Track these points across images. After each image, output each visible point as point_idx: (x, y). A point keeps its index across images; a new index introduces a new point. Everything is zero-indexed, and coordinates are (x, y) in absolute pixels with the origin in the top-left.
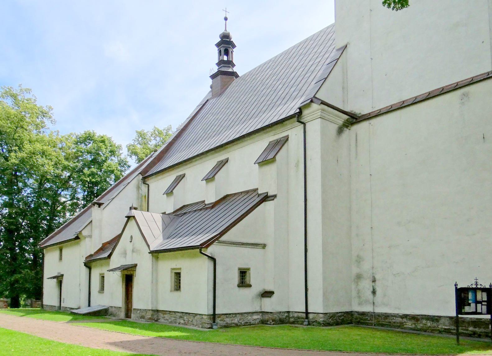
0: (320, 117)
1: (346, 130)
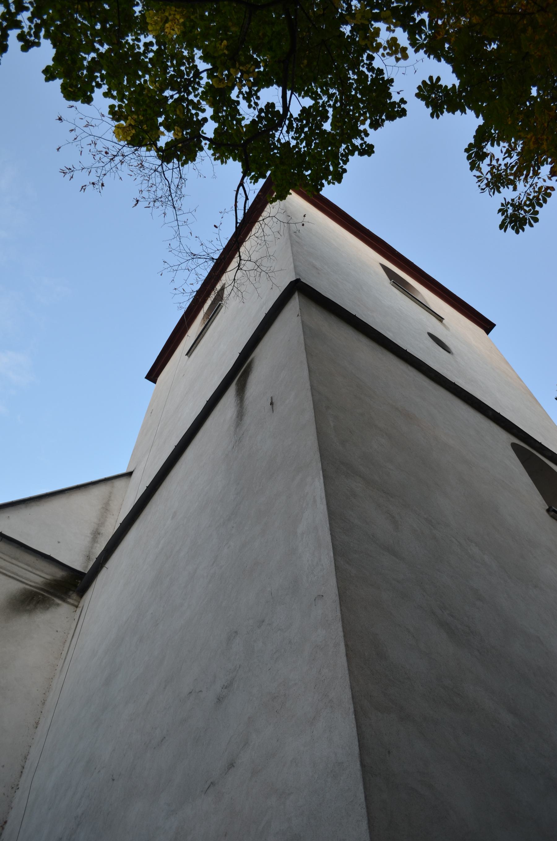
1: (58, 605)
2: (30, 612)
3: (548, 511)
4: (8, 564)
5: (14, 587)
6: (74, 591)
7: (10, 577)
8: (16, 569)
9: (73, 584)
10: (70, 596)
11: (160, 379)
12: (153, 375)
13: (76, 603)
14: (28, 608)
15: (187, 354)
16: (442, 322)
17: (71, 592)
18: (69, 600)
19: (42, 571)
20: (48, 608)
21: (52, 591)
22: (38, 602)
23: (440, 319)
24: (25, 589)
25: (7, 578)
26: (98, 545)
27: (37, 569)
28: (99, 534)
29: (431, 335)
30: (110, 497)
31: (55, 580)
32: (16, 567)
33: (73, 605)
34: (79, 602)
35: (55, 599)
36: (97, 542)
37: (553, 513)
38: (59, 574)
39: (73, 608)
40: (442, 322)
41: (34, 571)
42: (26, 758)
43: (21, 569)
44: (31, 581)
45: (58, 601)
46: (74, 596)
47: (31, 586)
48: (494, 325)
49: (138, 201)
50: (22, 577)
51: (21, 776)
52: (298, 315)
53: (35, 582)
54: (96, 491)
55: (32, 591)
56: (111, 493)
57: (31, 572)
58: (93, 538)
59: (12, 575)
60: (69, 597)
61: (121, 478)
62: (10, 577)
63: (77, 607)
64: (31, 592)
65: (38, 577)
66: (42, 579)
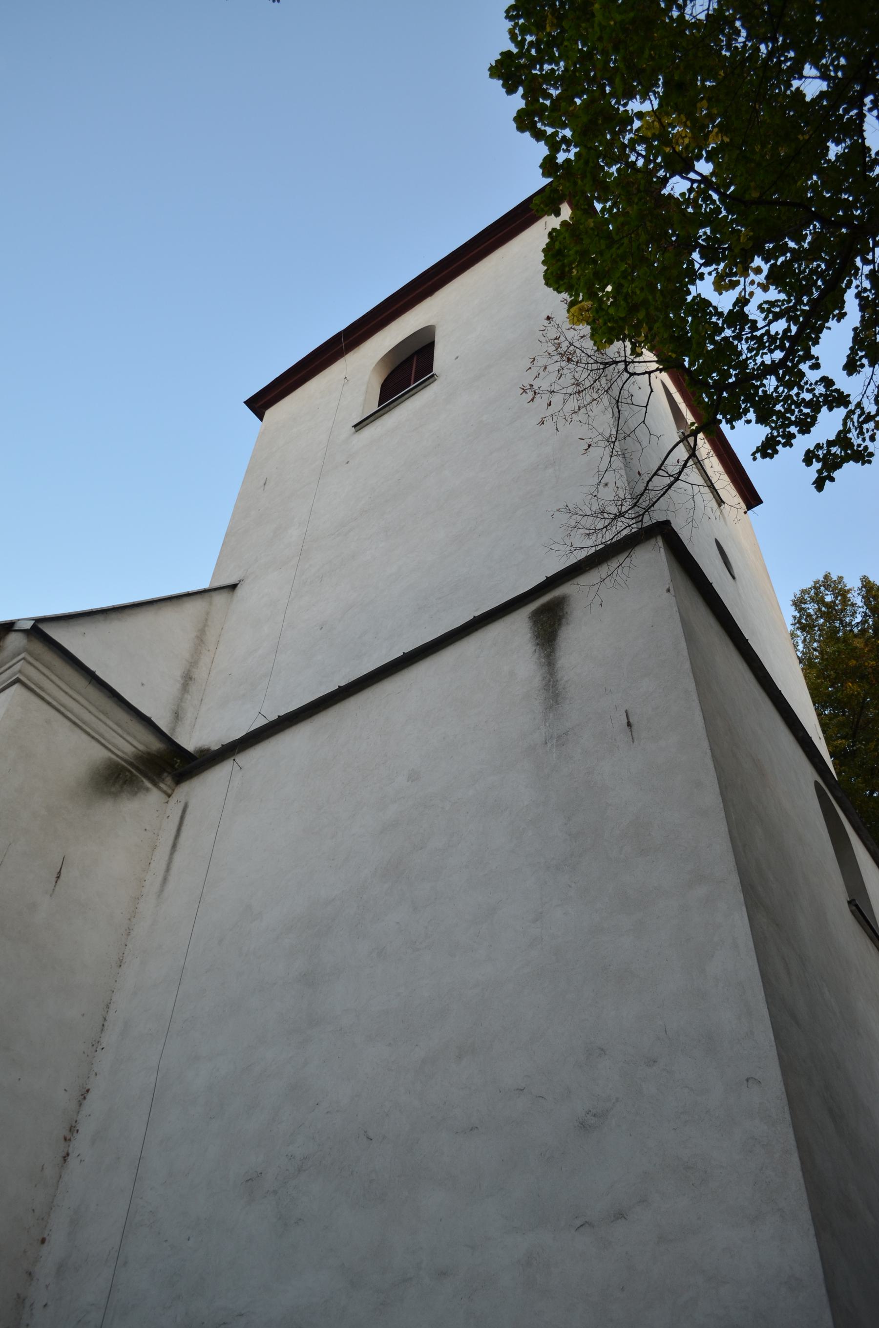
0: (18, 681)
1: (148, 790)
2: (116, 795)
3: (849, 903)
4: (94, 719)
5: (98, 754)
6: (169, 773)
7: (93, 737)
8: (102, 728)
9: (173, 764)
10: (163, 780)
11: (269, 413)
12: (260, 403)
13: (169, 792)
14: (113, 789)
15: (355, 426)
16: (720, 506)
17: (166, 774)
18: (162, 785)
19: (135, 737)
20: (136, 794)
21: (141, 767)
22: (125, 782)
23: (720, 502)
24: (110, 759)
25: (90, 739)
26: (189, 697)
27: (129, 734)
28: (191, 678)
29: (717, 542)
30: (206, 620)
31: (149, 754)
32: (104, 726)
33: (165, 792)
34: (173, 790)
35: (144, 780)
36: (188, 692)
37: (854, 908)
38: (156, 745)
39: (163, 796)
40: (720, 506)
41: (125, 736)
42: (108, 1007)
43: (108, 729)
44: (119, 750)
45: (148, 784)
46: (169, 780)
47: (117, 756)
48: (761, 502)
49: (589, 446)
50: (71, 712)
51: (102, 1030)
52: (668, 590)
53: (123, 752)
54: (193, 608)
55: (123, 767)
56: (208, 613)
57: (121, 736)
58: (183, 684)
59: (97, 736)
60: (163, 781)
61: (222, 591)
62: (93, 737)
63: (169, 796)
64: (117, 765)
65: (129, 746)
66: (133, 749)
